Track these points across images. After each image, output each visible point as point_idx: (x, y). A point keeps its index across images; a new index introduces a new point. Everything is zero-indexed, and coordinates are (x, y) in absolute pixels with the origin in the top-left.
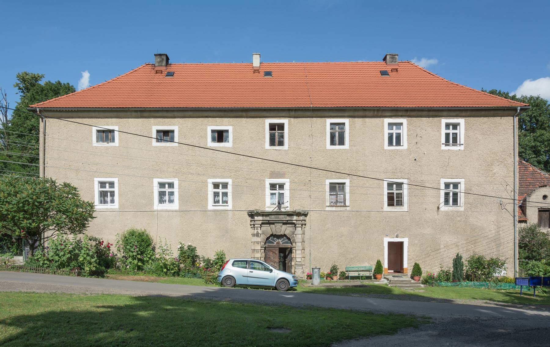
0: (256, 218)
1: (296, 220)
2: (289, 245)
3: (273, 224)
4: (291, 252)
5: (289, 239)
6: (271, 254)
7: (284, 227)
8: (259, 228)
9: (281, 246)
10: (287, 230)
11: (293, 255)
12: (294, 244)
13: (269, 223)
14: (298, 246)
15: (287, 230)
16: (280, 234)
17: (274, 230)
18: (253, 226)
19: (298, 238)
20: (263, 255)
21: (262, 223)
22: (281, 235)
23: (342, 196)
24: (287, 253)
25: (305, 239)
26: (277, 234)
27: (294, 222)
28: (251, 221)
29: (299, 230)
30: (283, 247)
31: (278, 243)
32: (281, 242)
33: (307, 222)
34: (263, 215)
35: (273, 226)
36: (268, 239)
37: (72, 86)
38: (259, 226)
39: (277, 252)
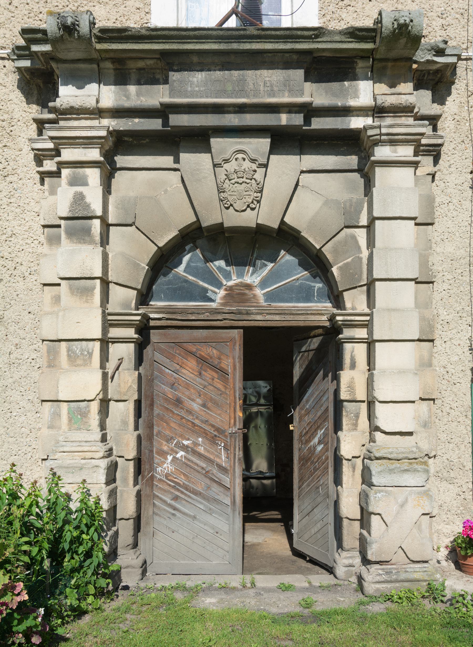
0: (68, 94)
1: (378, 111)
2: (318, 311)
3: (199, 139)
4: (328, 347)
5: (316, 263)
6: (189, 370)
7: (286, 166)
8: (93, 176)
9: (259, 320)
10: (301, 191)
11: (352, 380)
12: (355, 301)
13: (173, 137)
14: (396, 306)
15: (301, 191)
16: (248, 219)
17: (205, 191)
18: (49, 164)
19: (397, 247)
20: (126, 382)
21: (121, 143)
22: (260, 231)
23: (110, 310)
24: (297, 372)
25: (438, 263)
26: (233, 219)
27: (357, 123)
28: (41, 124)
29: (396, 187)
30: (276, 320)
31: (239, 295)
32: (267, 291)
33: (450, 130)
34: (121, 70)
35: (191, 160)
36: (163, 261)
37: (161, 104)
38: (94, 154)
39: (233, 361)
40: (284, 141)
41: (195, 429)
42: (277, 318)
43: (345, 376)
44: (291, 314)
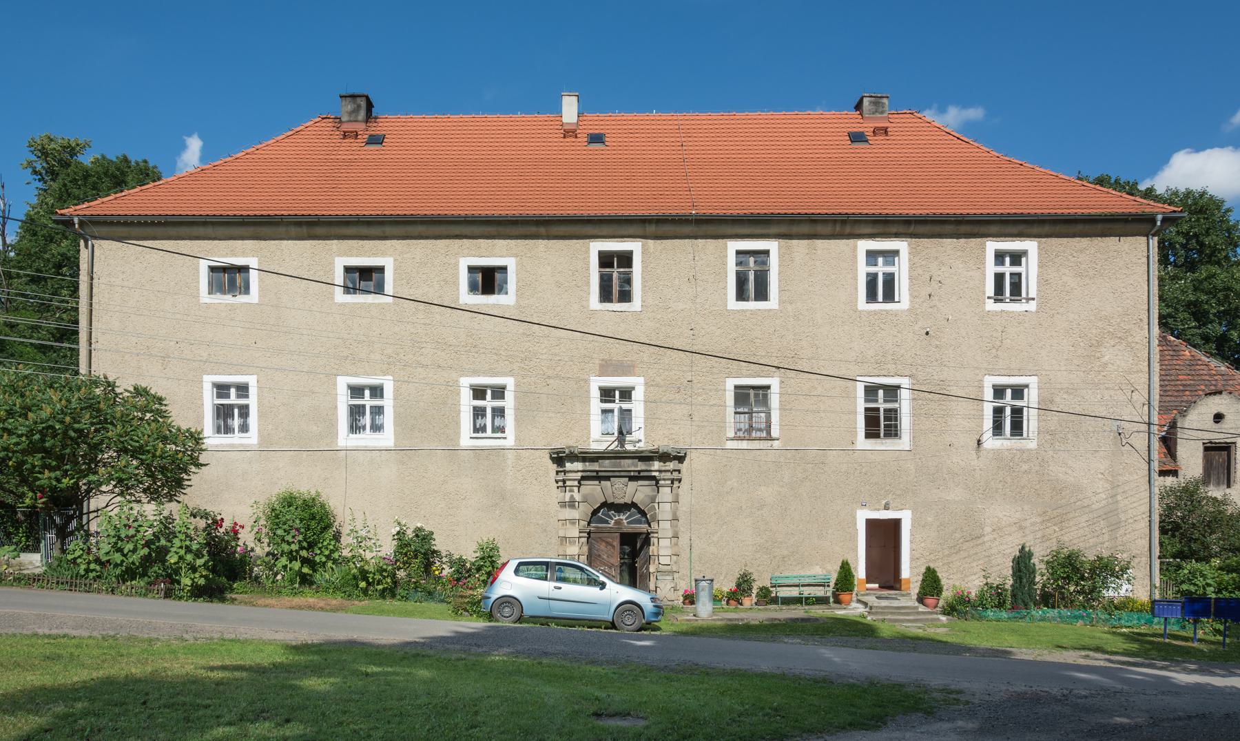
0: (569, 466)
1: (660, 471)
3: (608, 478)
4: (647, 541)
5: (643, 514)
6: (603, 546)
7: (633, 485)
8: (576, 489)
9: (625, 530)
10: (638, 492)
15: (638, 492)
16: (622, 501)
17: (609, 492)
18: (563, 485)
19: (664, 511)
20: (585, 549)
21: (583, 478)
25: (680, 514)
26: (617, 501)
28: (557, 472)
29: (665, 493)
30: (630, 531)
31: (618, 522)
33: (684, 475)
34: (584, 460)
36: (595, 512)
38: (576, 483)
39: (617, 543)
40: (632, 478)
41: (605, 564)
42: (1222, 436)
43: (651, 548)
44: (882, 613)
